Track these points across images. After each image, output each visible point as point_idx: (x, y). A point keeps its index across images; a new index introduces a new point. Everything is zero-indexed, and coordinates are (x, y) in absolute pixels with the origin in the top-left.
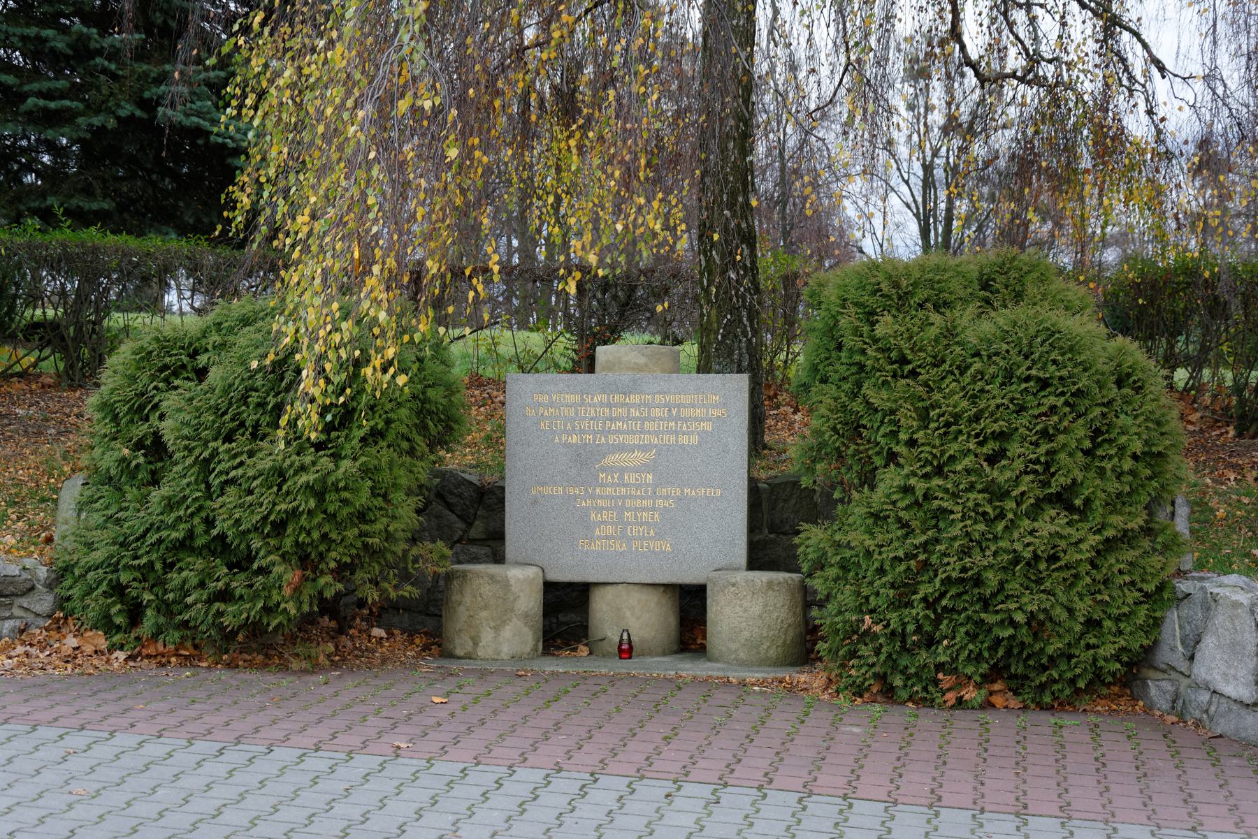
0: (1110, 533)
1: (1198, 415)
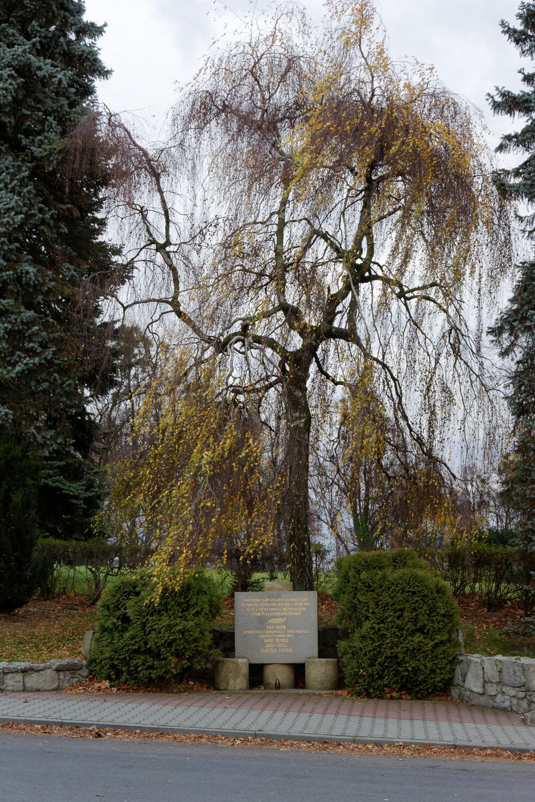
0: (436, 641)
1: (474, 604)
